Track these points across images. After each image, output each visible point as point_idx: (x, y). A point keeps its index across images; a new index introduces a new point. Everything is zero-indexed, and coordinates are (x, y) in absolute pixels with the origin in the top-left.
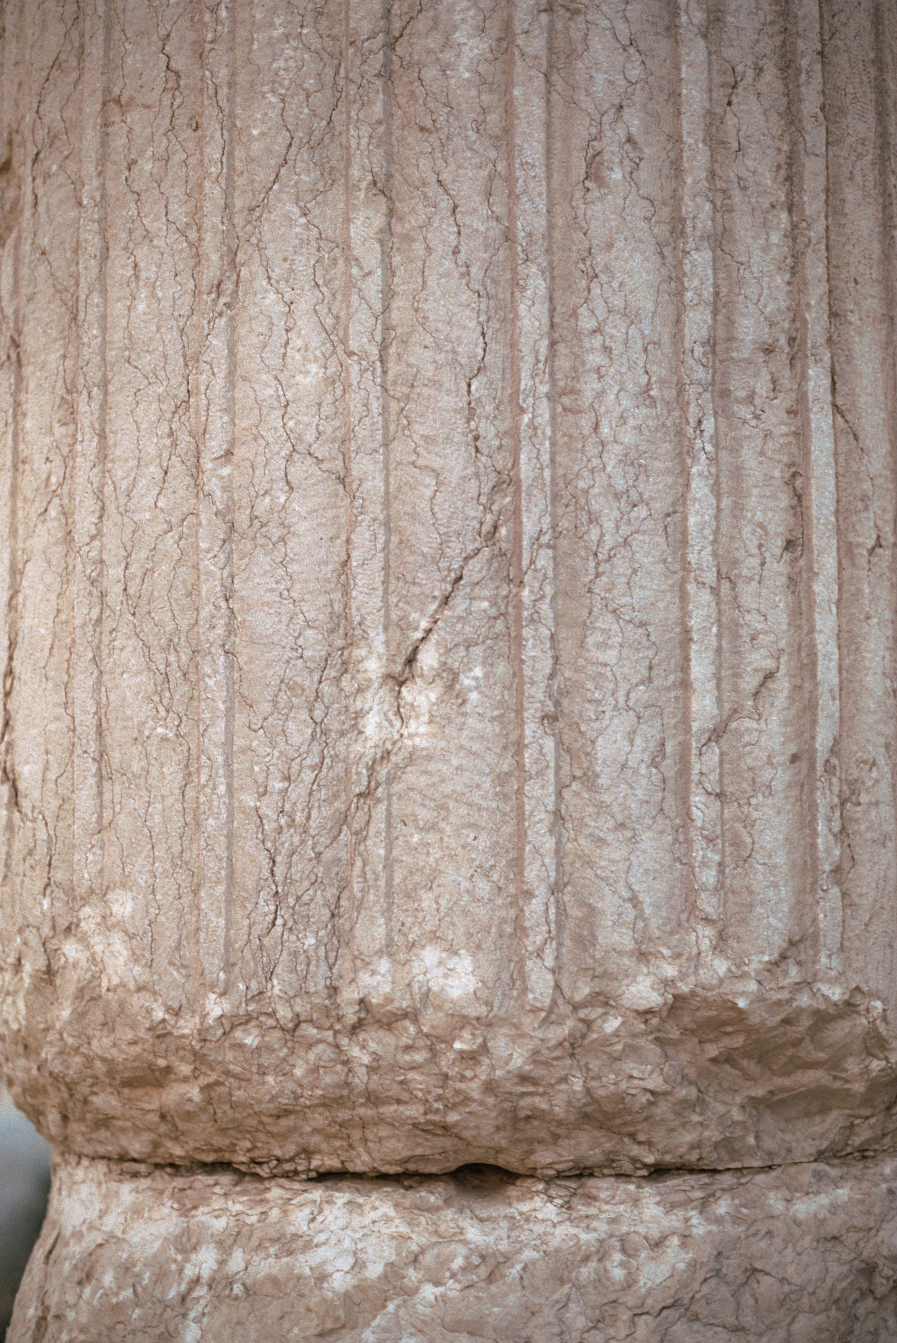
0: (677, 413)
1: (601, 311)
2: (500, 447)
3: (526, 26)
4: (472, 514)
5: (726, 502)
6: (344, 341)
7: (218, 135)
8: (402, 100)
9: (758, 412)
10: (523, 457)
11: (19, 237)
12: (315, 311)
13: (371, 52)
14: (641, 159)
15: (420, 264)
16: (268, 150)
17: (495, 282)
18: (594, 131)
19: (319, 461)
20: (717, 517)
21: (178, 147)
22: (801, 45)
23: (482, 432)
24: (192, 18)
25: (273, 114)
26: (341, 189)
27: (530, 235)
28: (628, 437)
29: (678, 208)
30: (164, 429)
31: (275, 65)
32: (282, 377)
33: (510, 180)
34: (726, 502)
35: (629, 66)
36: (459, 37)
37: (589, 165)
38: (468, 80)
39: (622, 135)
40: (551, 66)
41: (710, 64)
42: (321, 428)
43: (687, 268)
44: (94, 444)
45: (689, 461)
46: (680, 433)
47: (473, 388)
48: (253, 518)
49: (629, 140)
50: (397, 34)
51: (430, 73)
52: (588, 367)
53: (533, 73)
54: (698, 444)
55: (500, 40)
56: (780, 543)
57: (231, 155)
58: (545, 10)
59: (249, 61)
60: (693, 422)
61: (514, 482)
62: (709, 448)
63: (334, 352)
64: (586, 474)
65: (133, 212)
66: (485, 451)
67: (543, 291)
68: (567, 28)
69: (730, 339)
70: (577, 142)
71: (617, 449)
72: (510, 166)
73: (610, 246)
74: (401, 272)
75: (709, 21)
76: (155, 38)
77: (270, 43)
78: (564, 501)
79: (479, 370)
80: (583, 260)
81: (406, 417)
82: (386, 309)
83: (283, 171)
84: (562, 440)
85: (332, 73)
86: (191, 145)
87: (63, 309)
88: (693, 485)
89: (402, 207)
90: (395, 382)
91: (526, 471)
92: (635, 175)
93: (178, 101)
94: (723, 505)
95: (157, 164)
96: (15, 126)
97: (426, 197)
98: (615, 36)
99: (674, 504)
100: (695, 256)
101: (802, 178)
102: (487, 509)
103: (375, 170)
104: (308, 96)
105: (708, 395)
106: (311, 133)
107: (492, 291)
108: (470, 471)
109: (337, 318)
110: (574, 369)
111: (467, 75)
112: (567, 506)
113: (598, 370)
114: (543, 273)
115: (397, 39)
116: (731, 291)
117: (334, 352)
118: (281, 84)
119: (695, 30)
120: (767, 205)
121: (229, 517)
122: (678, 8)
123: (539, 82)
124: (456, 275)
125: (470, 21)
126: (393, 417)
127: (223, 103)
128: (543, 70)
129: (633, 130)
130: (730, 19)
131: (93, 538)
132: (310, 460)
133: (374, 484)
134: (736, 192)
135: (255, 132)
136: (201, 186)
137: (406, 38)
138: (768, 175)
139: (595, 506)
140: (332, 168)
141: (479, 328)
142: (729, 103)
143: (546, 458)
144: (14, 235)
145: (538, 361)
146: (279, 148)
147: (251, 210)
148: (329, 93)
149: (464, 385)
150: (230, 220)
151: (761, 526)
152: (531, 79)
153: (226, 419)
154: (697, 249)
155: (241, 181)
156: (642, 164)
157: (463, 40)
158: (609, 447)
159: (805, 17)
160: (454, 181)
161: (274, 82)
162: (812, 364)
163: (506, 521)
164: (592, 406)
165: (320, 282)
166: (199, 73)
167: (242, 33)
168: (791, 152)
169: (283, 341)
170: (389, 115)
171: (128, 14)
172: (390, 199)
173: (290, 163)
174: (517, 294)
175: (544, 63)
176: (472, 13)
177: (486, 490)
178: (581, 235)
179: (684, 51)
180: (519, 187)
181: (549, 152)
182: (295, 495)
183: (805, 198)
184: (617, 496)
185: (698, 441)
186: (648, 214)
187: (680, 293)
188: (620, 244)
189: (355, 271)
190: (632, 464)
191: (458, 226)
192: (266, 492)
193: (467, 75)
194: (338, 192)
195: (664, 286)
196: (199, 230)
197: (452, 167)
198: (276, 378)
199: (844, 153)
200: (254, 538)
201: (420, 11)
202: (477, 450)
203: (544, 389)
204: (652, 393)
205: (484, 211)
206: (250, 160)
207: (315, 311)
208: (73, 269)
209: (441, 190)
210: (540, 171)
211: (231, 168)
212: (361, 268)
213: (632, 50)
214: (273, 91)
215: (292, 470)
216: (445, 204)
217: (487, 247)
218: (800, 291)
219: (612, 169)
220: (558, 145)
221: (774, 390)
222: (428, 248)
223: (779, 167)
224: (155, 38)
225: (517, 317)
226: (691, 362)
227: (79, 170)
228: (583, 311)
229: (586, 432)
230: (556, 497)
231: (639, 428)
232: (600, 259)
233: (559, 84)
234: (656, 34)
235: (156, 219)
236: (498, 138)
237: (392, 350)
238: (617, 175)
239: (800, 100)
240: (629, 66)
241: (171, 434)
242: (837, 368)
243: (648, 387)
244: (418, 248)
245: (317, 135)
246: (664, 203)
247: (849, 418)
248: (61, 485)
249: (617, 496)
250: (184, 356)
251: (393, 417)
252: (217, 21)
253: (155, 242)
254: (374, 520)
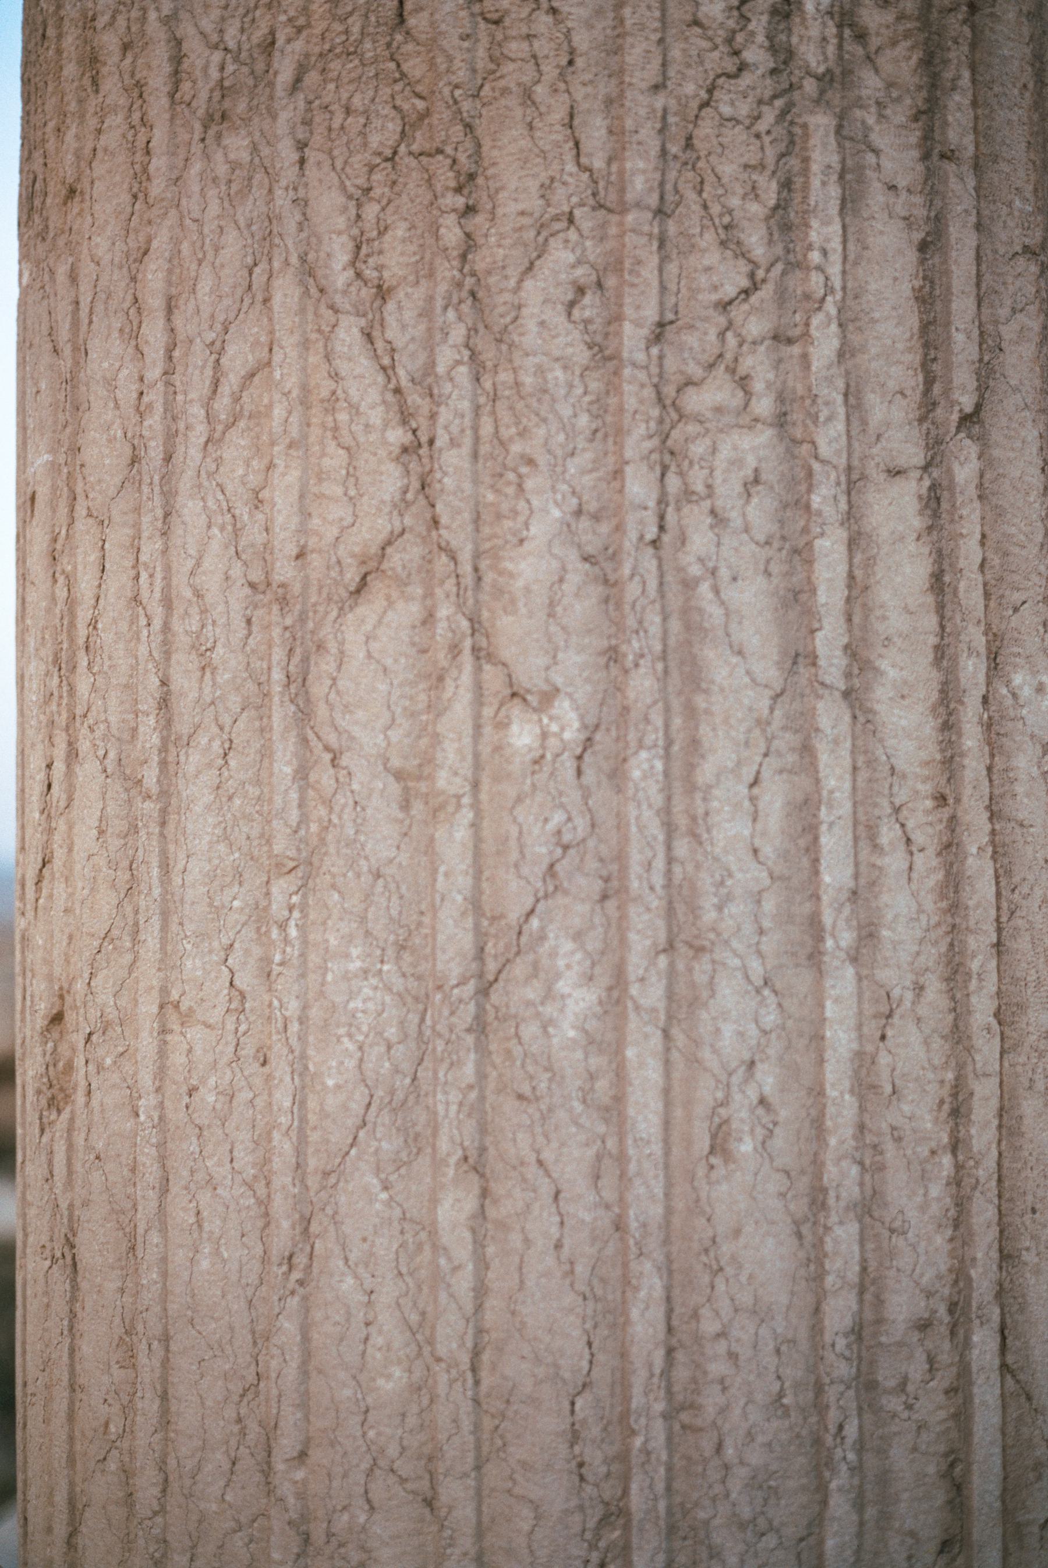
0: (814, 1419)
1: (724, 1306)
2: (608, 1475)
3: (641, 972)
4: (575, 1552)
5: (871, 1512)
6: (431, 1342)
7: (288, 1079)
8: (497, 1060)
9: (911, 1401)
10: (634, 1487)
11: (72, 1120)
12: (398, 1305)
13: (461, 1001)
14: (775, 1124)
15: (517, 1259)
16: (345, 1107)
17: (603, 1281)
18: (720, 1095)
19: (403, 1480)
20: (860, 1535)
21: (243, 1083)
22: (972, 943)
23: (587, 1459)
24: (258, 929)
25: (351, 1064)
26: (428, 1159)
27: (644, 1225)
28: (756, 1457)
29: (818, 1176)
30: (230, 1413)
31: (352, 1005)
32: (362, 1378)
33: (622, 1158)
34: (871, 1512)
35: (763, 1011)
36: (562, 986)
37: (714, 1136)
38: (574, 1041)
39: (753, 1095)
40: (670, 1017)
41: (860, 995)
42: (405, 1443)
43: (829, 1246)
44: (155, 1407)
45: (827, 1474)
46: (817, 1442)
47: (577, 1407)
48: (329, 1535)
49: (762, 1101)
50: (491, 978)
51: (530, 1030)
52: (710, 1376)
53: (649, 1029)
54: (839, 1453)
55: (610, 989)
56: (933, 1546)
57: (303, 1103)
58: (664, 951)
59: (322, 994)
60: (832, 1428)
61: (624, 1513)
62: (851, 1456)
63: (419, 1354)
64: (707, 1502)
65: (194, 1147)
66: (590, 1478)
67: (659, 1292)
68: (690, 970)
69: (879, 1321)
70: (701, 1110)
71: (743, 1472)
72: (621, 1141)
73: (737, 1232)
74: (495, 1264)
75: (860, 938)
76: (216, 944)
77: (346, 977)
78: (681, 1533)
79: (584, 1386)
80: (706, 1251)
81: (502, 1437)
82: (479, 1308)
83: (362, 1134)
84: (679, 1463)
85: (417, 1020)
86: (258, 1082)
87: (121, 1234)
88: (832, 1502)
89: (497, 1188)
90: (488, 1395)
91: (637, 1501)
92: (768, 1143)
93: (243, 1028)
94: (867, 1516)
95: (221, 1098)
96: (66, 986)
97: (524, 1180)
98: (747, 977)
99: (810, 1525)
100: (839, 1231)
101: (970, 1110)
102: (593, 1546)
103: (466, 1143)
104: (389, 1047)
105: (851, 1393)
106: (392, 1092)
107: (599, 1292)
108: (574, 1503)
109: (423, 1314)
110: (694, 1380)
111: (572, 1033)
112: (685, 1538)
113: (722, 1381)
114: (659, 1269)
115: (491, 984)
116: (881, 1264)
117: (419, 1354)
118: (359, 1029)
119: (842, 955)
120: (926, 1153)
121: (304, 1528)
122: (823, 930)
123: (656, 1040)
124: (559, 1274)
125: (576, 968)
126: (486, 1436)
127: (294, 1041)
128: (661, 1024)
129: (767, 1090)
130: (885, 933)
131: (156, 1513)
132: (392, 1479)
133: (465, 1514)
134: (889, 1146)
135: (330, 1083)
136: (269, 1133)
137: (501, 983)
138: (928, 1117)
139: (717, 1539)
140: (417, 1136)
141: (585, 1338)
142: (883, 1037)
143: (660, 1487)
144: (65, 1115)
145: (652, 1375)
146: (356, 1107)
147: (326, 1174)
148: (413, 1045)
149: (566, 1405)
150: (302, 1181)
151: (912, 1534)
152: (646, 1036)
153: (299, 1415)
154: (841, 1223)
155: (314, 1137)
156: (777, 1131)
157: (567, 990)
158: (735, 1470)
159: (978, 906)
160: (557, 1161)
161: (350, 1025)
162: (976, 1329)
163: (614, 1559)
164: (714, 1423)
165: (404, 1270)
166: (266, 997)
167: (314, 959)
168: (957, 1079)
169: (363, 1336)
170: (482, 1076)
171: (187, 906)
172: (482, 1176)
173: (369, 1126)
174: (629, 1294)
175: (663, 1017)
176: (578, 956)
177: (591, 1524)
178: (704, 1221)
179: (828, 983)
180: (632, 1168)
181: (667, 1124)
182: (377, 1517)
183: (973, 1131)
184: (742, 1526)
185: (839, 1450)
186: (783, 1189)
187: (819, 1277)
188: (749, 1228)
189: (442, 1261)
190: (760, 1487)
191: (560, 1214)
192: (345, 1508)
193: (572, 1033)
194: (423, 1163)
195: (802, 1272)
196: (268, 1184)
197: (555, 1145)
198: (354, 1377)
199: (1022, 1059)
200: (332, 1558)
201: (518, 953)
202: (582, 1479)
203: (659, 1407)
204: (785, 1401)
205: (592, 1198)
206: (324, 1115)
207: (398, 1305)
208: (130, 1190)
209: (541, 1172)
210: (657, 1148)
211: (303, 1120)
212: (449, 1259)
213: (766, 992)
214: (350, 1036)
215: (372, 1486)
216: (546, 1188)
217: (594, 1239)
218: (964, 1243)
219: (740, 1140)
220: (678, 1113)
221: (930, 1370)
222: (527, 1241)
223: (942, 1102)
224: (216, 944)
225: (627, 1322)
226: (832, 1357)
227: (136, 1073)
228: (705, 1312)
229: (707, 1454)
230: (672, 1530)
231: (769, 1445)
232: (726, 1249)
233: (680, 1038)
234: (797, 965)
235: (220, 1164)
236: (607, 1109)
237: (486, 1357)
238: (746, 1147)
239: (969, 1012)
240: (763, 1011)
241: (239, 1420)
242: (1008, 1321)
243: (781, 1395)
244: (515, 1239)
245: (400, 1095)
246: (803, 1172)
247: (1021, 1377)
248: (121, 1437)
249: (742, 1526)
250: (253, 1332)
251: (486, 1436)
252: (286, 941)
253: (219, 1191)
254: (465, 1554)
